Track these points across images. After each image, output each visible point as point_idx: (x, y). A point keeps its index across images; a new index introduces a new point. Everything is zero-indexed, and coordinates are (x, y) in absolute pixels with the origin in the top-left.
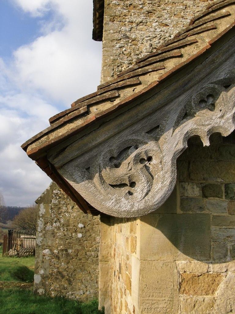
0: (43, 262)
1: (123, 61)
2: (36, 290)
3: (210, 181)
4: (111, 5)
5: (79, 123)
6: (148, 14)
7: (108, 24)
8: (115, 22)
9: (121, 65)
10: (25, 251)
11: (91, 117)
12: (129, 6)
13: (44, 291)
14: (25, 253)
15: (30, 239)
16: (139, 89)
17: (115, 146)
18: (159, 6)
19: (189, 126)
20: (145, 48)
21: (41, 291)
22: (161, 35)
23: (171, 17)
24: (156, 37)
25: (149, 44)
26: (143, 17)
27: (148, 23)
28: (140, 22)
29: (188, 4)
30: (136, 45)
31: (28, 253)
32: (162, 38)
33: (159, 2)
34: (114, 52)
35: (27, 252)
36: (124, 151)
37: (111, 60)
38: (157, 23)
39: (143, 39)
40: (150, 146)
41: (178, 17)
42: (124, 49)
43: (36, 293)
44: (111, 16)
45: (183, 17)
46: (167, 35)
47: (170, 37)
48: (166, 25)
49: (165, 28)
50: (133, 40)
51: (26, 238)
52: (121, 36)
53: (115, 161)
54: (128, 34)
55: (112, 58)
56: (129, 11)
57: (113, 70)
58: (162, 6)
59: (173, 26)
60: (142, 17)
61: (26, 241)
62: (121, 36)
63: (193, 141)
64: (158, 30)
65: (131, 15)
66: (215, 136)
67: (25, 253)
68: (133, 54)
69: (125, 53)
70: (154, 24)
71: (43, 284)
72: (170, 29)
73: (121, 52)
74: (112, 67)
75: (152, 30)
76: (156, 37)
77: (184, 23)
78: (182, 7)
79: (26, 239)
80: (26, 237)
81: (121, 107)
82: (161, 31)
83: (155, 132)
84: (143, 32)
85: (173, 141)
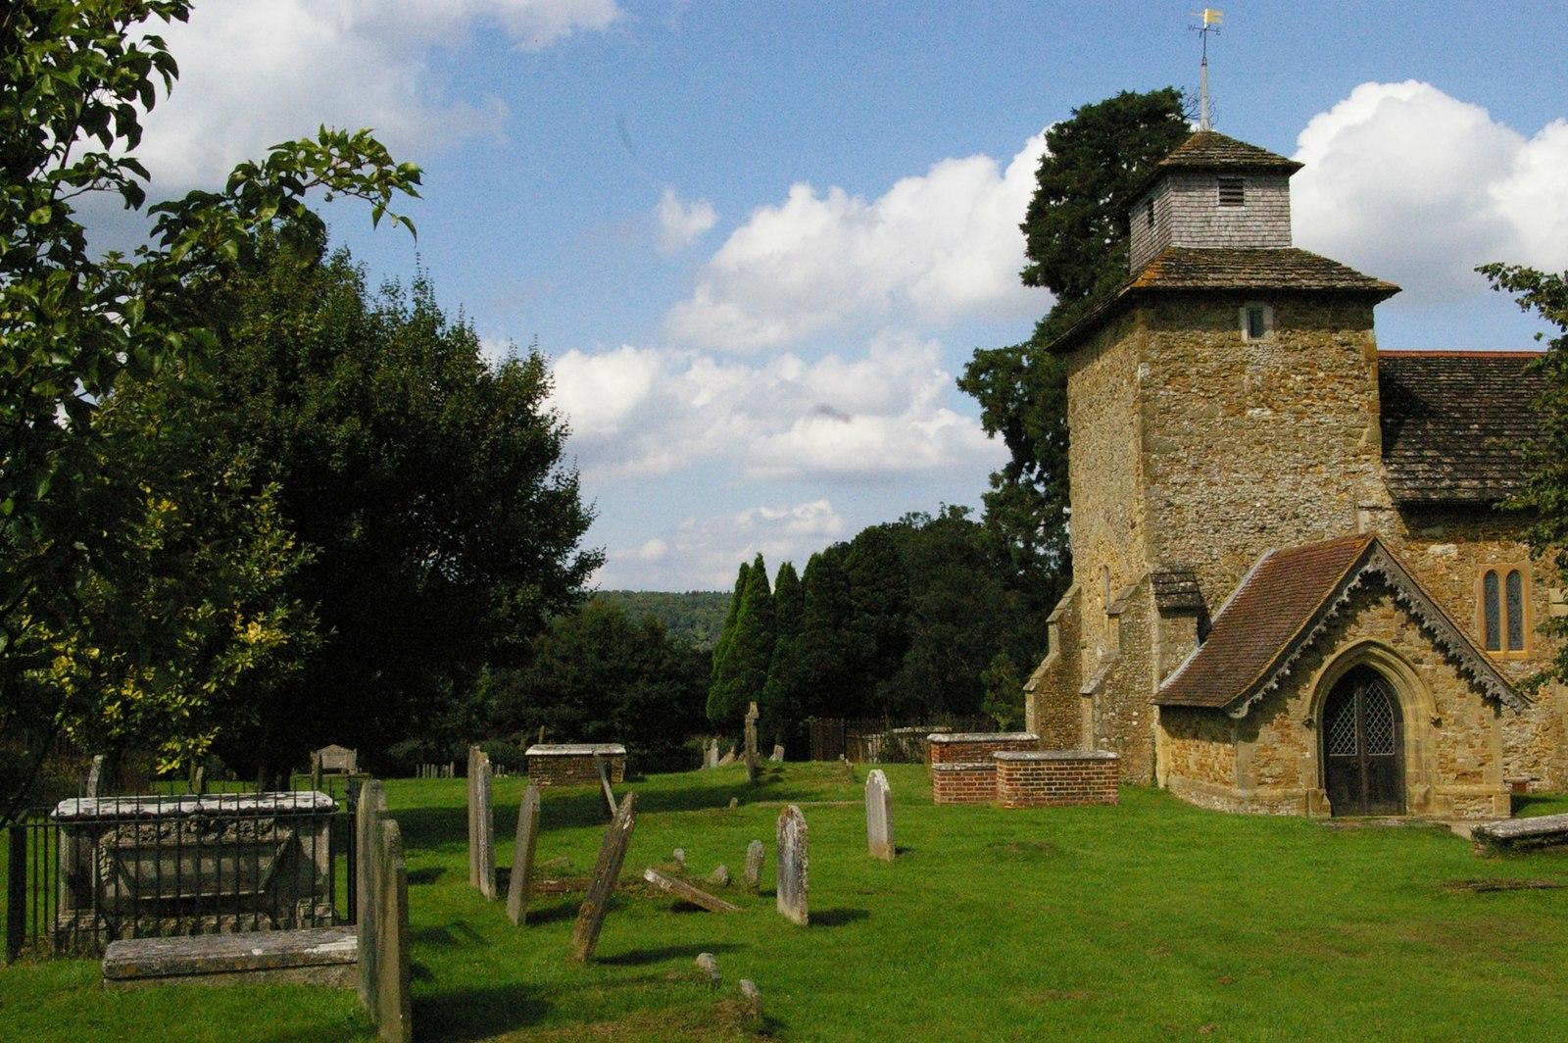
54: (1172, 500)
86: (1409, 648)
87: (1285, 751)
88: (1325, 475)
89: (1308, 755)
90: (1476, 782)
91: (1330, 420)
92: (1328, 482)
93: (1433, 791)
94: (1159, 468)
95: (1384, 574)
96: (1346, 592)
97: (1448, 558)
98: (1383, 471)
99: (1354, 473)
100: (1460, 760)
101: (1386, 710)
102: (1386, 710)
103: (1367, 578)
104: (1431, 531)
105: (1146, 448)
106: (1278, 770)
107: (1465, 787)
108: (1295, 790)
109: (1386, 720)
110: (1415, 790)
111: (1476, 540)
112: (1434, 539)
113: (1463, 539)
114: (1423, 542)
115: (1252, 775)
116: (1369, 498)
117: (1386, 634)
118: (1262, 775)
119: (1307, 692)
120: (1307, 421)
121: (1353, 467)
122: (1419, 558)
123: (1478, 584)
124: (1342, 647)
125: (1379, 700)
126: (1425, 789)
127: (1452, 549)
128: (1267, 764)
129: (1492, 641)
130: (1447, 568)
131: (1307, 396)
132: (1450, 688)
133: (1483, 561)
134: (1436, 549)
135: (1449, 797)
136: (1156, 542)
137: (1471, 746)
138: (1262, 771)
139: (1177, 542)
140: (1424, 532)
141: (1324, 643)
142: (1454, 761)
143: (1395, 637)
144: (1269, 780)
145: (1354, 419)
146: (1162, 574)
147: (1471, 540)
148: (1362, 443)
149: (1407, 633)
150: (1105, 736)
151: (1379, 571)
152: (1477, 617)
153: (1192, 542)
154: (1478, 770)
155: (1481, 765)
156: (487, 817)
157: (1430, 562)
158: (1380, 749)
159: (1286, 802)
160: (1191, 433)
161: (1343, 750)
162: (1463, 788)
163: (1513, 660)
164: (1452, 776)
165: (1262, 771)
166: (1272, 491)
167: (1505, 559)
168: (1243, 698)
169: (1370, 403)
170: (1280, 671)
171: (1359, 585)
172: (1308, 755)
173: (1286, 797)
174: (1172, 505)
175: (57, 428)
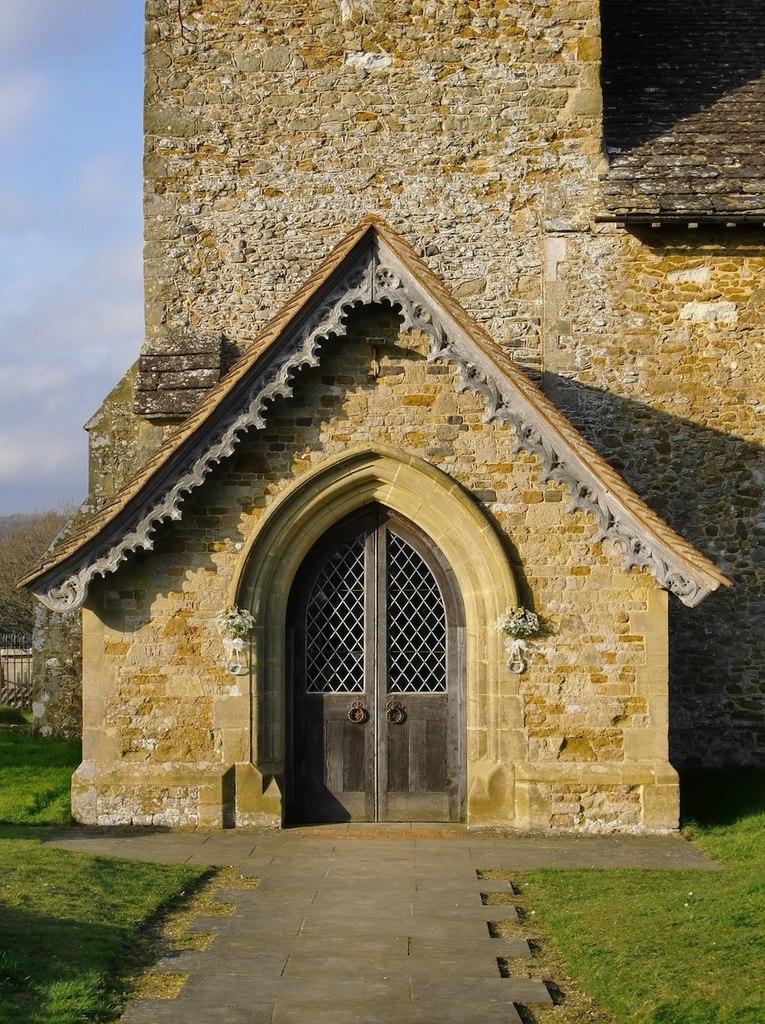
0: (47, 680)
1: (184, 288)
2: (37, 729)
3: (126, 589)
4: (157, 150)
5: (39, 573)
6: (239, 165)
7: (152, 200)
8: (166, 194)
9: (181, 295)
10: (11, 698)
11: (44, 570)
12: (198, 148)
13: (50, 730)
14: (10, 702)
15: (24, 660)
16: (65, 556)
17: (57, 580)
18: (264, 143)
19: (94, 568)
20: (229, 254)
21: (46, 730)
22: (266, 218)
23: (290, 169)
24: (255, 223)
25: (238, 243)
26: (225, 178)
27: (239, 190)
28: (221, 191)
29: (330, 133)
30: (212, 246)
31: (20, 703)
32: (267, 226)
33: (265, 133)
34: (166, 267)
35: (18, 699)
36: (61, 583)
37: (160, 288)
38: (258, 189)
39: (228, 231)
40: (73, 579)
41: (305, 168)
42: (186, 260)
43: (37, 733)
44: (158, 180)
45: (314, 169)
46: (280, 216)
47: (287, 220)
48: (277, 192)
49: (272, 202)
50: (206, 236)
51: (11, 657)
52: (181, 228)
53: (58, 586)
54: (195, 221)
55: (161, 282)
56: (197, 164)
57: (165, 309)
58: (271, 142)
59: (292, 195)
60: (225, 175)
61: (11, 666)
62: (181, 228)
63: (97, 575)
64: (260, 207)
65: (201, 174)
66: (108, 573)
67: (13, 703)
68: (205, 269)
69: (188, 268)
70: (250, 194)
71: (49, 719)
72: (285, 201)
73: (180, 267)
74: (162, 304)
75: (246, 207)
76: (255, 223)
77: (318, 182)
78: (314, 142)
79: (12, 660)
80: (11, 652)
81: (57, 566)
82: (266, 208)
83: (76, 572)
84: (227, 215)
85: (85, 575)
86: (465, 468)
87: (184, 683)
88: (488, 176)
89: (235, 691)
90: (608, 755)
91: (503, 75)
92: (491, 189)
93: (509, 774)
94: (175, 163)
95: (398, 307)
96: (309, 343)
97: (719, 327)
98: (603, 166)
99: (547, 171)
100: (571, 709)
101: (431, 601)
102: (431, 601)
103: (358, 315)
104: (687, 276)
105: (151, 128)
106: (167, 723)
108: (202, 765)
109: (431, 621)
110: (477, 772)
112: (693, 293)
115: (111, 732)
116: (568, 215)
117: (413, 437)
118: (134, 732)
119: (230, 559)
120: (458, 76)
121: (545, 160)
122: (663, 328)
125: (417, 580)
126: (493, 769)
130: (717, 345)
131: (461, 30)
132: (553, 553)
134: (696, 311)
135: (541, 788)
136: (164, 300)
137: (597, 680)
139: (201, 299)
141: (255, 458)
142: (558, 709)
143: (433, 444)
144: (149, 744)
145: (549, 73)
146: (163, 356)
148: (565, 115)
149: (463, 435)
150: (56, 653)
151: (385, 301)
153: (233, 297)
155: (616, 720)
157: (682, 337)
158: (417, 683)
159: (178, 791)
160: (235, 98)
161: (417, 683)
162: (576, 767)
164: (554, 742)
166: (388, 205)
168: (72, 565)
169: (581, 41)
170: (159, 512)
171: (340, 331)
172: (235, 691)
174: (195, 230)
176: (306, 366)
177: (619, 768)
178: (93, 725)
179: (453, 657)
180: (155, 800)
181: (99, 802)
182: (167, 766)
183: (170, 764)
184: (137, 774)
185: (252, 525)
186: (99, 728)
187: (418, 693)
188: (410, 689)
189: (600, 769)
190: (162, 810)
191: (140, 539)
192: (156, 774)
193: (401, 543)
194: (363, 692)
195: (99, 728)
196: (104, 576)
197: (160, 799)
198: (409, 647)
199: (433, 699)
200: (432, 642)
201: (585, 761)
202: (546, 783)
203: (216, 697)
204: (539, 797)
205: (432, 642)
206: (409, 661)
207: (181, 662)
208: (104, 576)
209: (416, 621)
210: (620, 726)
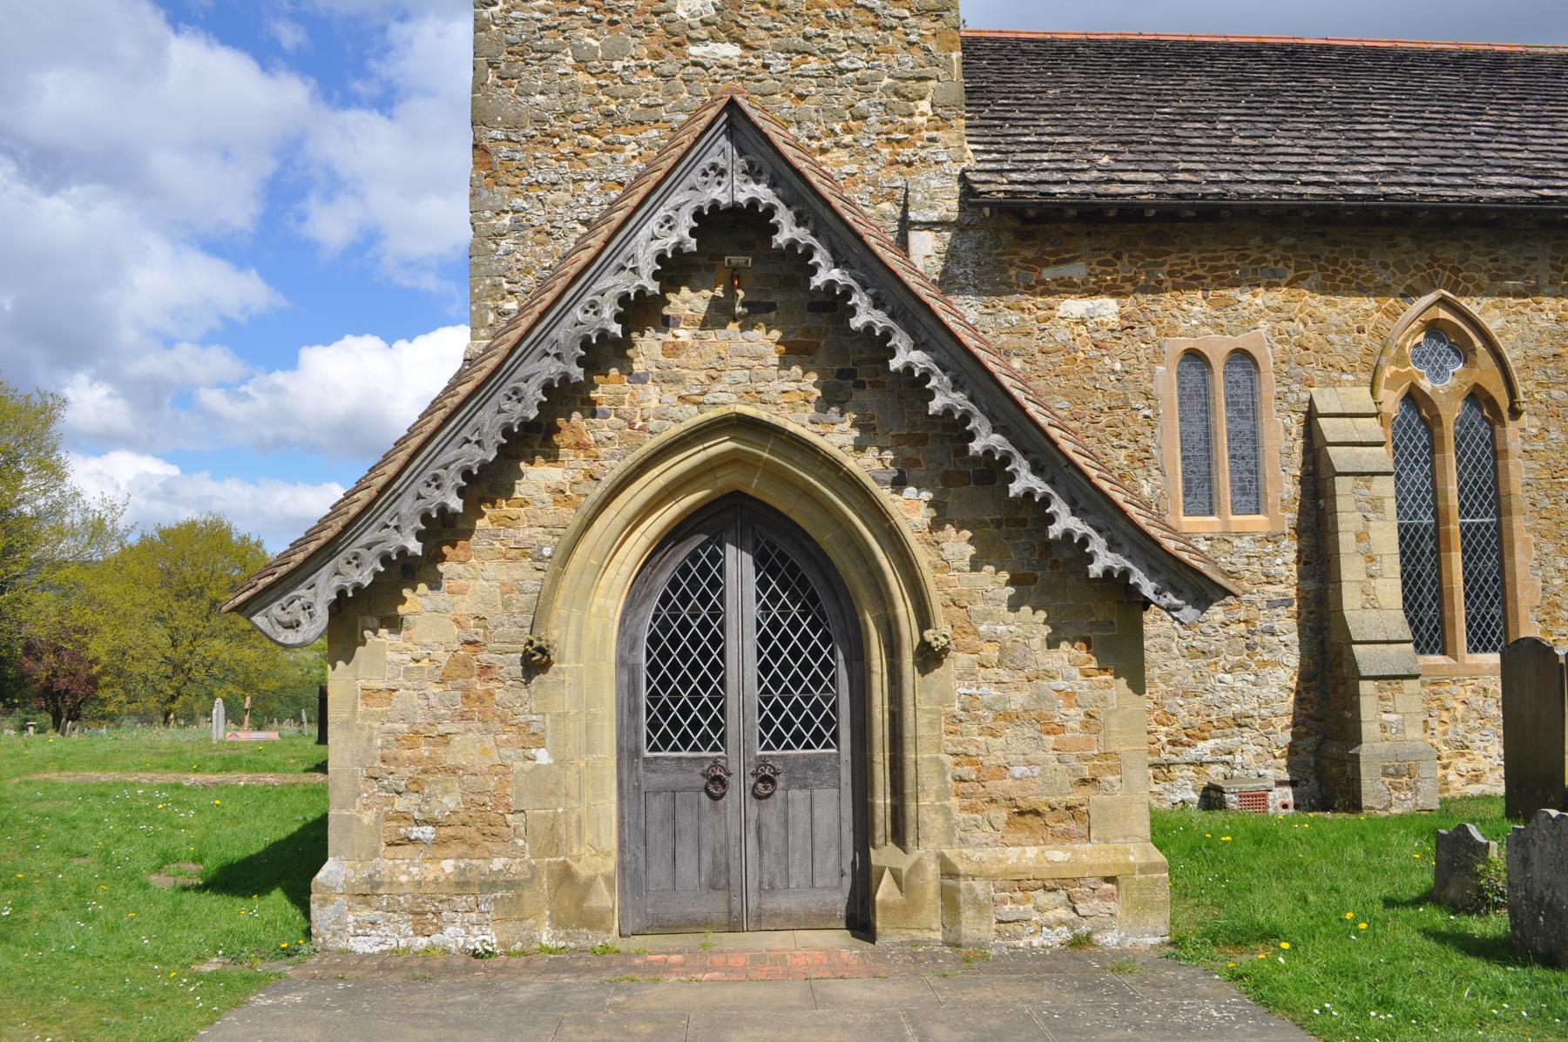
66: (358, 588)
87: (470, 747)
90: (1067, 836)
91: (854, 60)
99: (910, 164)
104: (1065, 271)
106: (450, 802)
107: (1031, 852)
108: (498, 864)
111: (1157, 289)
112: (1068, 287)
113: (1128, 287)
114: (1049, 293)
115: (368, 818)
118: (404, 817)
121: (907, 153)
123: (1166, 379)
124: (910, 509)
127: (1107, 308)
128: (415, 786)
129: (1200, 494)
133: (1171, 331)
134: (1074, 306)
138: (400, 804)
140: (1048, 274)
144: (427, 832)
147: (1144, 290)
152: (1169, 445)
154: (1074, 798)
156: (1451, 576)
157: (1062, 335)
159: (460, 902)
162: (1027, 855)
163: (1239, 535)
165: (400, 804)
167: (1220, 329)
173: (462, 884)
175: (1007, 490)
176: (775, 229)
177: (1087, 855)
178: (342, 807)
179: (634, 712)
180: (430, 916)
181: (351, 918)
182: (448, 866)
183: (452, 862)
184: (404, 879)
185: (836, 437)
186: (352, 812)
187: (819, 750)
188: (789, 746)
189: (1058, 855)
190: (440, 929)
191: (906, 355)
192: (431, 877)
193: (773, 548)
194: (647, 754)
195: (352, 812)
196: (350, 594)
197: (437, 914)
198: (675, 691)
199: (822, 757)
200: (705, 683)
201: (1036, 845)
202: (987, 878)
203: (518, 765)
204: (976, 898)
205: (705, 683)
206: (787, 708)
207: (463, 717)
208: (350, 594)
209: (795, 653)
210: (1095, 797)
